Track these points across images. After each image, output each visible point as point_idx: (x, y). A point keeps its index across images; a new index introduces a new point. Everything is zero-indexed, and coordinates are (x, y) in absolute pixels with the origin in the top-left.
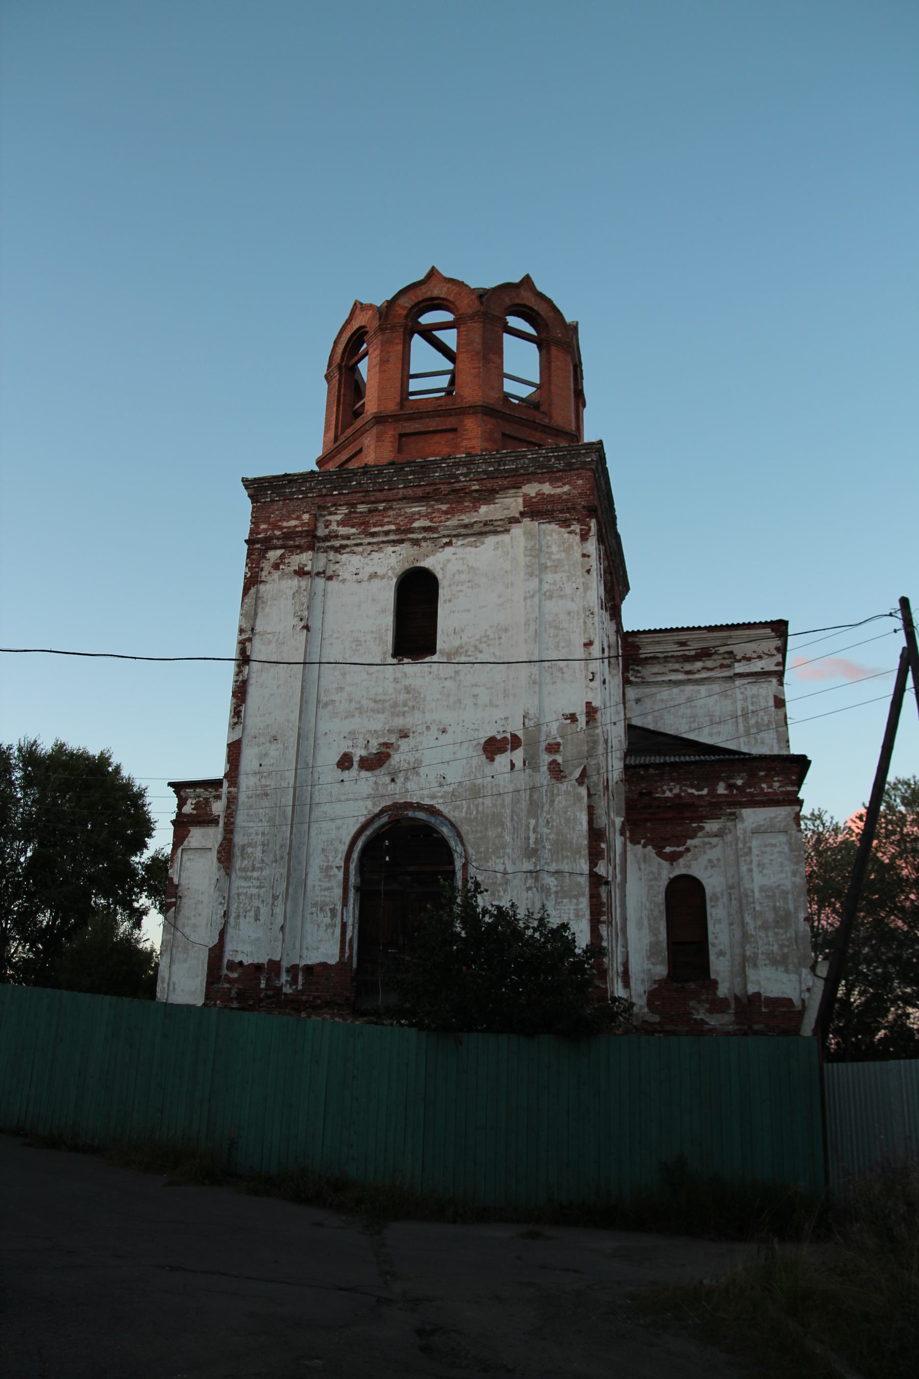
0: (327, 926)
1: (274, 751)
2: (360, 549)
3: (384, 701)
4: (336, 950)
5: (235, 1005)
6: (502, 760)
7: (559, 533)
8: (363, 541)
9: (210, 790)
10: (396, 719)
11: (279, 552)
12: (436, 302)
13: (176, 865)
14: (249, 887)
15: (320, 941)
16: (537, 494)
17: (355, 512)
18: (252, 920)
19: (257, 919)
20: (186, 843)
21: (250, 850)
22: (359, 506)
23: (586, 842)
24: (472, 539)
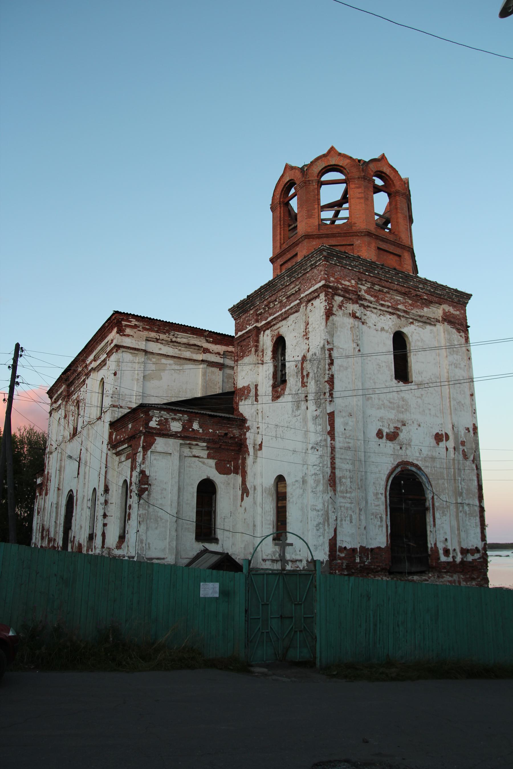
1: (351, 422)
2: (375, 311)
3: (394, 403)
5: (346, 573)
6: (442, 444)
7: (457, 335)
9: (171, 414)
11: (341, 299)
12: (383, 175)
13: (147, 462)
14: (345, 503)
15: (377, 535)
16: (448, 312)
17: (373, 288)
18: (349, 522)
19: (351, 522)
20: (153, 447)
21: (344, 480)
22: (376, 286)
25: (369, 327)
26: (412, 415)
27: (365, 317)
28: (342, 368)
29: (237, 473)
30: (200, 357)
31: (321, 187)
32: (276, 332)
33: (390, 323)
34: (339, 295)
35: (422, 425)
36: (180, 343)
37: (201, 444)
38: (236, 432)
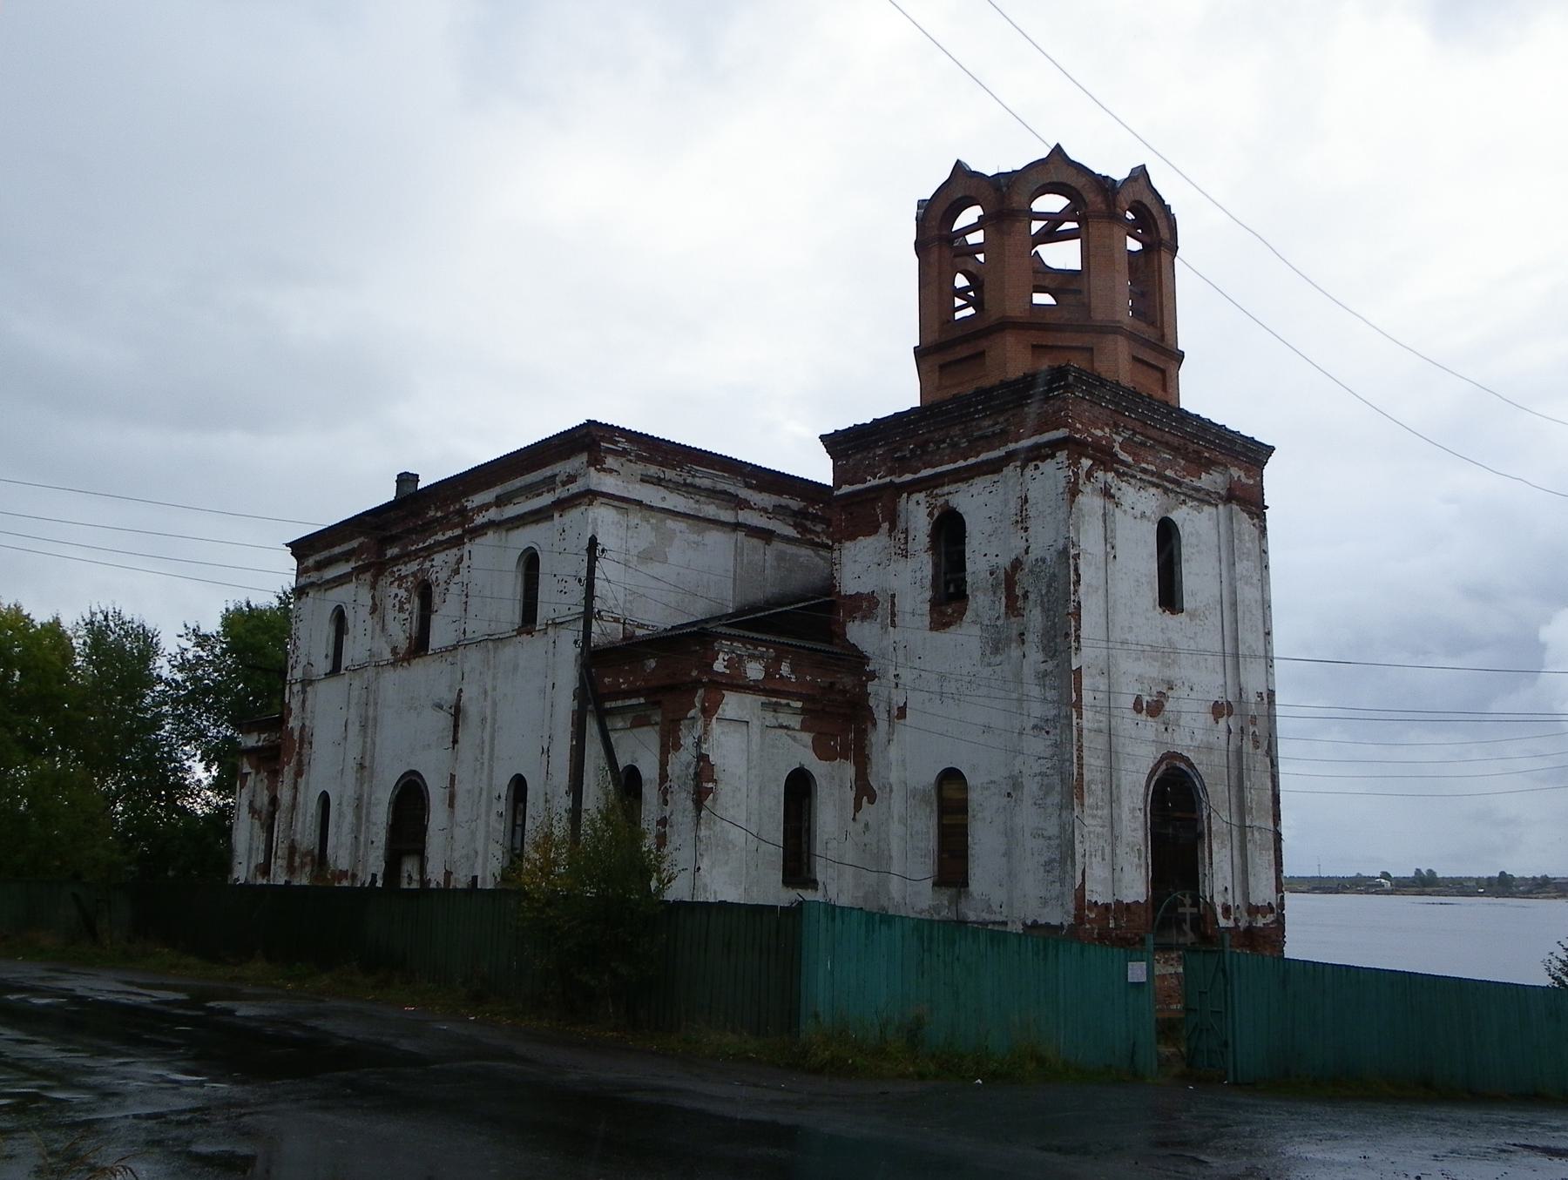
2: (1133, 481)
11: (1090, 462)
30: (727, 516)
32: (941, 501)
33: (1154, 503)
34: (1087, 457)
38: (847, 681)
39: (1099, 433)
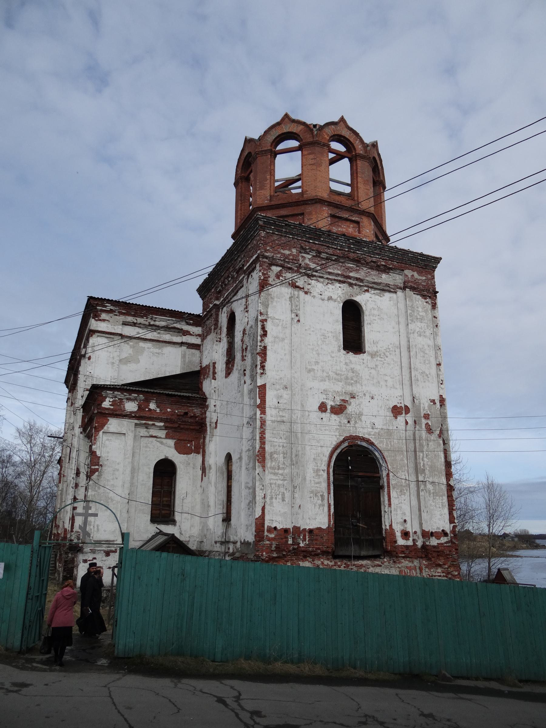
0: (320, 505)
2: (322, 280)
3: (341, 375)
4: (326, 520)
6: (401, 419)
8: (324, 276)
9: (125, 394)
10: (348, 387)
11: (279, 269)
13: (98, 443)
14: (277, 480)
15: (316, 514)
18: (280, 501)
19: (283, 500)
20: (105, 428)
21: (275, 456)
23: (444, 468)
24: (379, 292)
25: (314, 297)
26: (364, 387)
27: (309, 287)
28: (277, 340)
29: (198, 453)
31: (276, 157)
32: (230, 308)
33: (340, 292)
35: (375, 397)
36: (158, 326)
37: (158, 424)
38: (197, 411)
39: (287, 252)
